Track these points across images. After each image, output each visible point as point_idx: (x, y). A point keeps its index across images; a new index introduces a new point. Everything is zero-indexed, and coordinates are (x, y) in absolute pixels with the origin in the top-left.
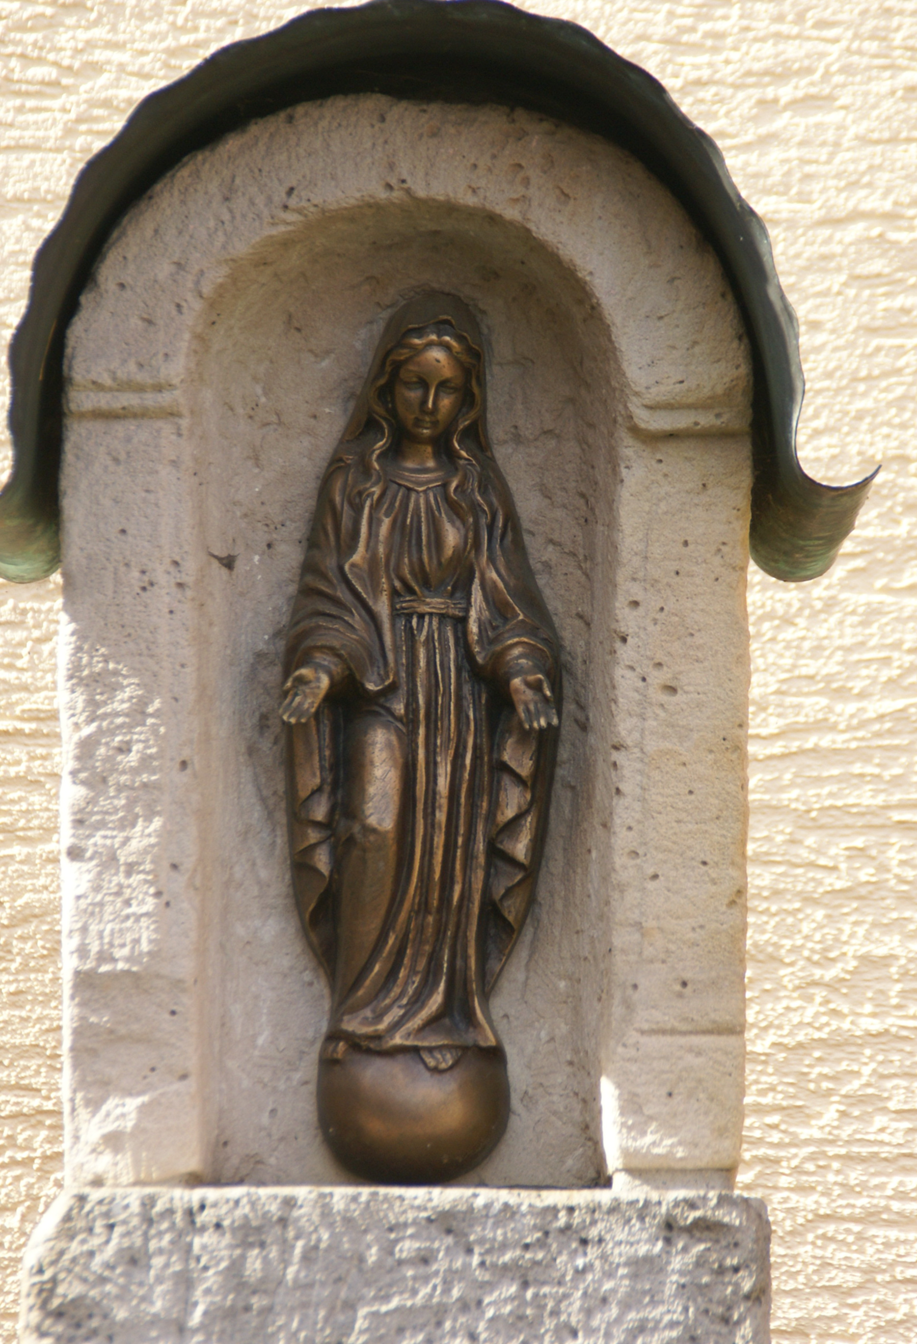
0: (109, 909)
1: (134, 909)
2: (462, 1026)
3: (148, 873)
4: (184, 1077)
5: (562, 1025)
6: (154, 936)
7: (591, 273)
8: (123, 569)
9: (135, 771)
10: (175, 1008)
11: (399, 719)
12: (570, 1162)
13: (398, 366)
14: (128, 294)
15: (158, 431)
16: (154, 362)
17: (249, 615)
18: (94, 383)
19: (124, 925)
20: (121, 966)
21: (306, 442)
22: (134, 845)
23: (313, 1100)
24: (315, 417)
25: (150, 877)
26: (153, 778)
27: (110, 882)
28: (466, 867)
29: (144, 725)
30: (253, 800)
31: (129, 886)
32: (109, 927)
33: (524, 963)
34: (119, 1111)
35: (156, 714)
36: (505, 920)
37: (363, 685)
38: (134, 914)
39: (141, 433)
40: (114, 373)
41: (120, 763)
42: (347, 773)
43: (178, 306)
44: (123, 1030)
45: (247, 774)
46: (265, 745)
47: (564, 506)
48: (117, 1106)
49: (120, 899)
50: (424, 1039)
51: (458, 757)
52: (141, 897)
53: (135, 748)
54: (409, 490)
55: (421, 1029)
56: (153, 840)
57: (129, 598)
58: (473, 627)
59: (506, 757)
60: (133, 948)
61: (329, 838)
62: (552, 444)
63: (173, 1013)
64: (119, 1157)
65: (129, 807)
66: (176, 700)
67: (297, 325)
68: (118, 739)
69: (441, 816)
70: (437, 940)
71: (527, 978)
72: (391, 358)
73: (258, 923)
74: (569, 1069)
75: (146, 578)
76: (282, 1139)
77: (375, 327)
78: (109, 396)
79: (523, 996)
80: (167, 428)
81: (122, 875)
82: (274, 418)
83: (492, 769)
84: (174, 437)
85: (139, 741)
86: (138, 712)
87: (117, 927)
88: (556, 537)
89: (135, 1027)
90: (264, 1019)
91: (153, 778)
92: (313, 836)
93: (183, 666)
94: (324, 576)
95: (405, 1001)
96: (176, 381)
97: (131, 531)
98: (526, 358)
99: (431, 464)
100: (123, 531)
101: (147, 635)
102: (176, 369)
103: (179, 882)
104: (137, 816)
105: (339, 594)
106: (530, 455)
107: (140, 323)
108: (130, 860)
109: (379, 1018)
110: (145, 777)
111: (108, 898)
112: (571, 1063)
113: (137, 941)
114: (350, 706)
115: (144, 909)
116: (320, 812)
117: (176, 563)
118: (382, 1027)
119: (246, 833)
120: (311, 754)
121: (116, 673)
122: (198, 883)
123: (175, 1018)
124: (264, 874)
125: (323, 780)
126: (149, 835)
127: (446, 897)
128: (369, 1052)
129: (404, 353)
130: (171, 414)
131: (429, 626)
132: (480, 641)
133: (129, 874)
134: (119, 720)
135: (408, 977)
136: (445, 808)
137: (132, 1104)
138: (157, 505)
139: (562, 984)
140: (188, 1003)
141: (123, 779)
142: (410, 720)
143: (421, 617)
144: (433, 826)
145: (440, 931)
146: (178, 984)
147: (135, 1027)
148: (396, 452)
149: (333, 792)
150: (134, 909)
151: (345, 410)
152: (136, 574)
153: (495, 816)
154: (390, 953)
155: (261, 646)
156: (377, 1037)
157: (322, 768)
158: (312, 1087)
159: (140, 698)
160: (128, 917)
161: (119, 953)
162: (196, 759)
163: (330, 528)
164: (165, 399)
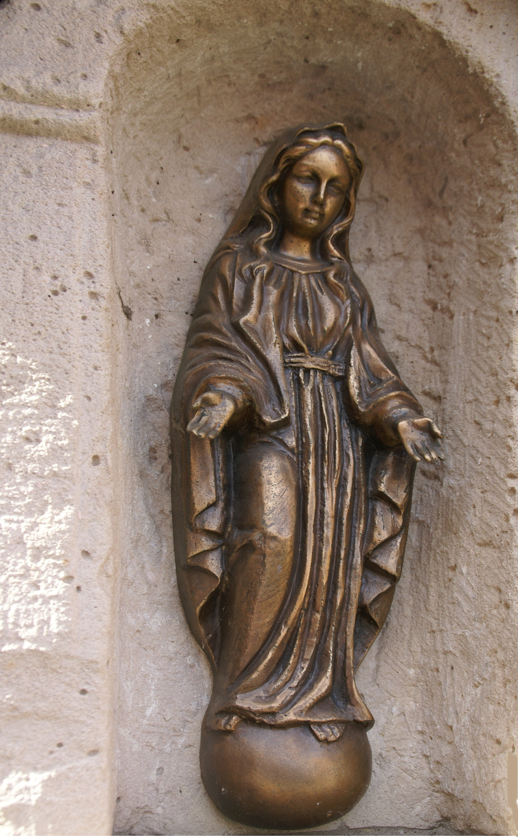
0: (13, 591)
1: (42, 591)
2: (340, 703)
3: (58, 558)
4: (94, 752)
5: (412, 703)
6: (64, 618)
7: (498, 76)
8: (32, 272)
9: (44, 460)
10: (86, 687)
11: (292, 450)
12: (418, 808)
13: (294, 161)
14: (43, 15)
15: (74, 152)
16: (71, 79)
17: (141, 365)
18: (5, 88)
19: (30, 607)
20: (26, 645)
21: (189, 240)
22: (42, 530)
23: (197, 760)
24: (199, 220)
25: (60, 562)
26: (64, 468)
27: (15, 564)
28: (346, 575)
29: (55, 418)
30: (144, 515)
31: (37, 569)
32: (14, 607)
33: (374, 654)
34: (23, 784)
35: (68, 409)
36: (372, 619)
37: (260, 417)
38: (42, 596)
39: (55, 152)
40: (28, 82)
41: (26, 452)
42: (241, 492)
43: (98, 36)
44: (27, 708)
45: (139, 492)
46: (154, 472)
47: (411, 311)
48: (20, 780)
49: (25, 582)
50: (315, 715)
51: (341, 487)
52: (50, 580)
53: (44, 439)
54: (293, 272)
55: (311, 708)
56: (63, 527)
57: (38, 299)
58: (353, 383)
59: (382, 488)
60: (41, 628)
61: (221, 546)
62: (401, 264)
63: (84, 692)
64: (21, 829)
65: (39, 491)
66: (89, 398)
67: (185, 143)
68: (25, 429)
69: (328, 532)
70: (322, 634)
71: (378, 667)
72: (286, 155)
73: (146, 615)
74: (419, 737)
75: (58, 283)
76: (168, 792)
77: (252, 158)
78: (21, 107)
79: (375, 680)
80: (82, 153)
81: (28, 558)
82: (164, 216)
83: (367, 499)
84: (88, 163)
85: (47, 432)
86: (50, 405)
87: (24, 608)
88: (403, 334)
89: (42, 705)
90: (152, 693)
91: (64, 468)
92: (206, 544)
93: (96, 368)
94: (218, 331)
95: (295, 683)
96: (95, 102)
97: (43, 237)
98: (380, 197)
99: (307, 256)
100: (34, 238)
101: (59, 334)
102: (96, 89)
103: (90, 570)
104: (46, 503)
105: (234, 344)
106: (380, 272)
107: (56, 44)
108: (37, 544)
109: (272, 697)
110: (55, 467)
111: (12, 580)
112: (422, 733)
113: (47, 622)
114: (245, 434)
115: (54, 592)
116: (213, 523)
117: (89, 275)
118: (275, 705)
119: (137, 541)
120: (207, 474)
121: (23, 367)
122: (110, 572)
123: (86, 696)
124: (151, 576)
125: (218, 498)
126: (60, 522)
127: (330, 600)
128: (262, 725)
129: (302, 149)
130: (87, 138)
131: (316, 379)
132: (360, 394)
133: (36, 558)
134: (27, 412)
135: (297, 663)
136: (331, 526)
137: (37, 779)
138: (70, 218)
139: (412, 672)
140: (99, 683)
141: (30, 467)
142: (301, 453)
143: (307, 371)
144: (321, 540)
145: (325, 625)
146: (90, 665)
147: (42, 705)
148: (277, 244)
149: (226, 508)
150: (42, 591)
151: (225, 220)
152: (46, 278)
153: (371, 536)
154: (282, 642)
155: (151, 392)
156: (273, 714)
157: (216, 486)
158: (196, 750)
159: (50, 393)
160: (35, 599)
161: (23, 633)
162: (109, 456)
163: (220, 296)
164: (83, 118)
